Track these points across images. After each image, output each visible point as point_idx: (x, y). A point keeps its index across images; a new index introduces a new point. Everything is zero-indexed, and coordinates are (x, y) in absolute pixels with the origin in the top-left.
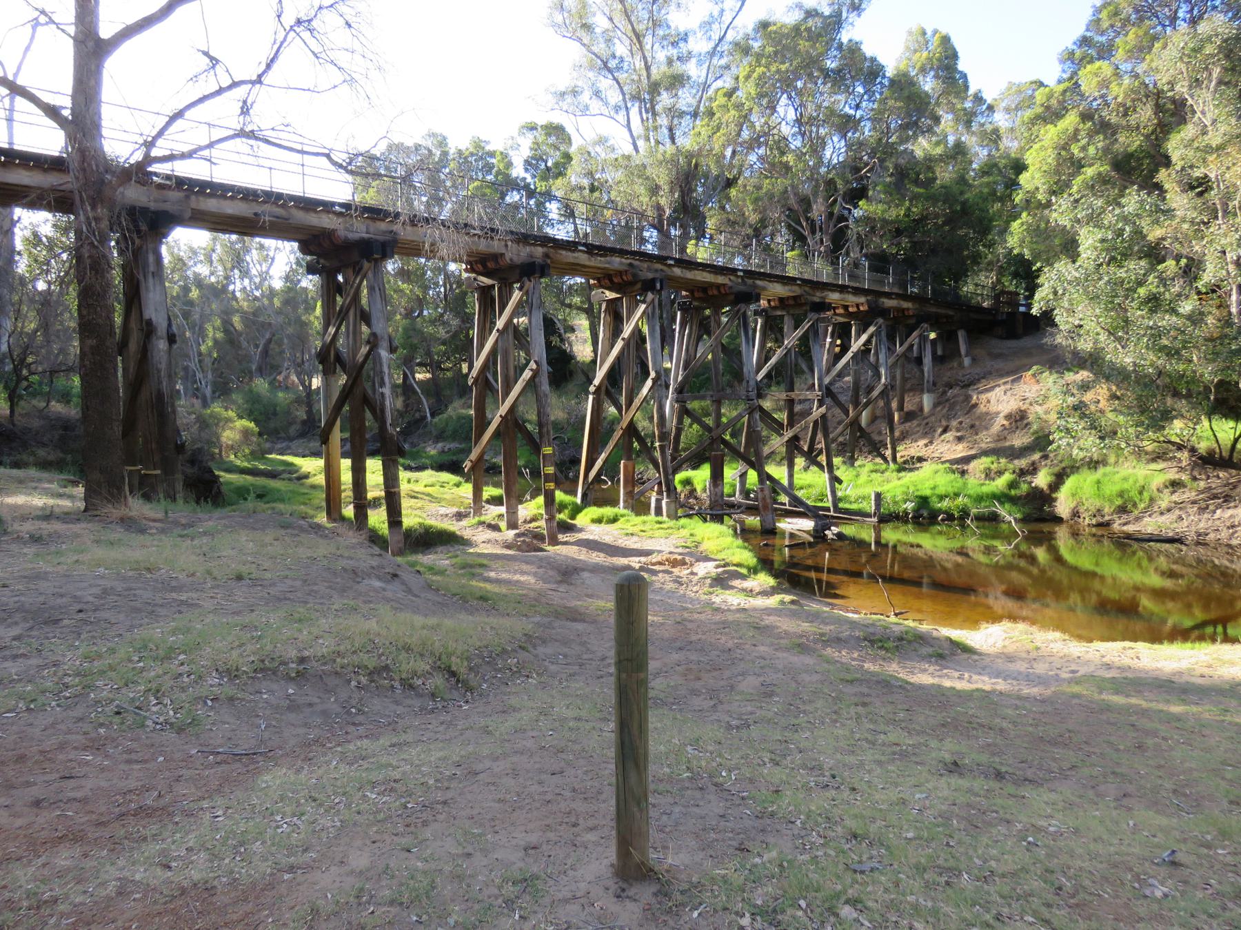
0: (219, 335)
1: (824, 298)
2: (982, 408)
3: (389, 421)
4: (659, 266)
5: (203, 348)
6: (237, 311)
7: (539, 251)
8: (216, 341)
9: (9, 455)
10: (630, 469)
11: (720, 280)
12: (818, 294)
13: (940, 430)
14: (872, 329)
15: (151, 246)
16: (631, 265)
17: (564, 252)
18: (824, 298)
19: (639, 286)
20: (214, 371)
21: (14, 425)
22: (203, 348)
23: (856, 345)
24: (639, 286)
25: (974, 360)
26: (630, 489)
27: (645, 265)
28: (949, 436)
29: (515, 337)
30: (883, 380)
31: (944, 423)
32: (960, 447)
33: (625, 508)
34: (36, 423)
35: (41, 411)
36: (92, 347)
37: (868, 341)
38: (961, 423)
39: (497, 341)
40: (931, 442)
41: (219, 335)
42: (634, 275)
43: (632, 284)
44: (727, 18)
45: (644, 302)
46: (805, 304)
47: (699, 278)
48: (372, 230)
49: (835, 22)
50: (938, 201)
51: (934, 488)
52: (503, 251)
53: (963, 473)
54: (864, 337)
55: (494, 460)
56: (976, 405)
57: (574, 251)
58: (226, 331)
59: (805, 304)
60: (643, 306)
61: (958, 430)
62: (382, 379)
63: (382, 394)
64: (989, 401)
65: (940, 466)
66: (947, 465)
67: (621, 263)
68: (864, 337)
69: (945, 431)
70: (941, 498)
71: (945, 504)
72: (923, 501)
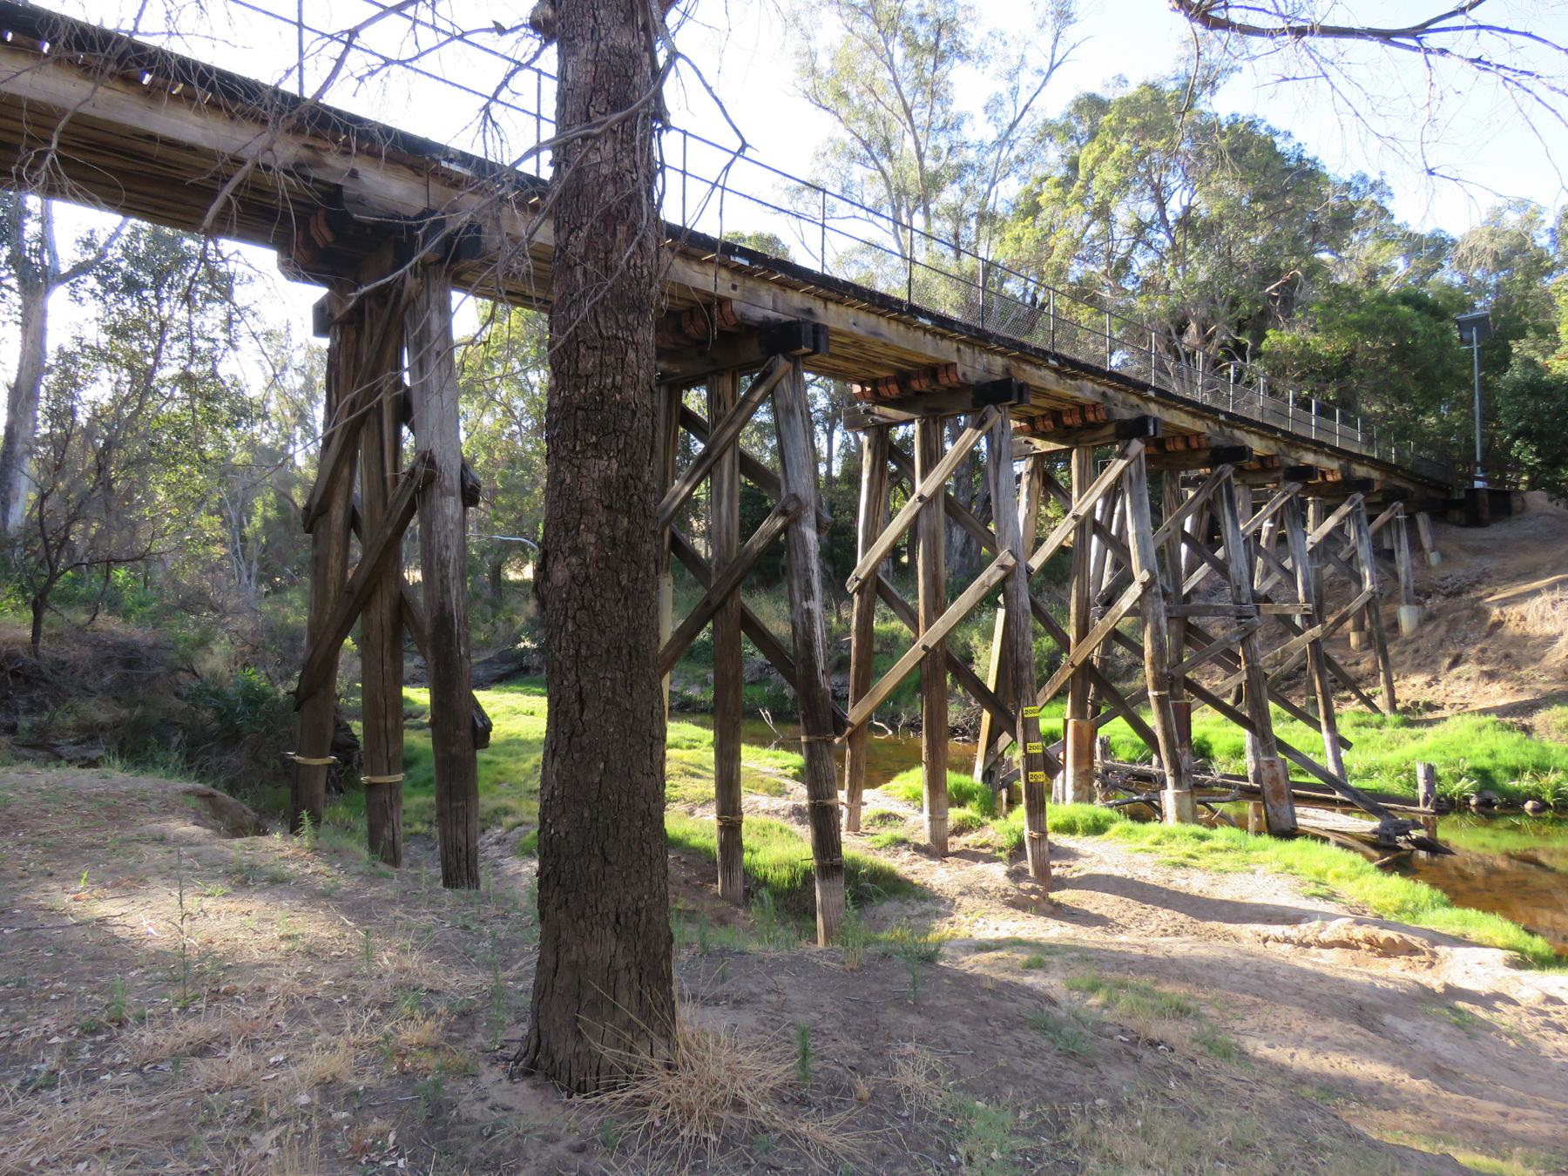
0: (271, 514)
1: (1297, 460)
2: (1512, 629)
3: (821, 666)
4: (1134, 400)
5: (247, 530)
6: (299, 481)
7: (998, 363)
8: (266, 520)
9: (29, 712)
10: (1086, 733)
11: (1198, 426)
12: (1293, 454)
13: (1447, 661)
14: (1345, 509)
15: (434, 296)
16: (1104, 394)
17: (1028, 368)
18: (1297, 460)
19: (1110, 430)
20: (260, 560)
21: (37, 656)
22: (247, 530)
23: (1315, 534)
24: (1110, 430)
25: (1443, 556)
26: (1086, 767)
27: (1120, 396)
28: (1469, 668)
29: (947, 510)
30: (1368, 585)
31: (1454, 651)
32: (1496, 687)
33: (1077, 800)
34: (75, 653)
35: (80, 629)
36: (606, 484)
37: (1339, 528)
38: (1483, 651)
39: (917, 516)
40: (1436, 680)
41: (271, 514)
42: (1109, 412)
43: (1095, 426)
44: (1023, 99)
45: (1122, 455)
46: (1278, 468)
47: (1176, 422)
48: (780, 305)
49: (1188, 94)
50: (1377, 332)
51: (1492, 755)
52: (955, 360)
53: (1527, 730)
54: (1331, 522)
55: (689, 693)
56: (1499, 624)
57: (1039, 367)
58: (280, 509)
59: (1278, 468)
60: (1121, 464)
61: (1481, 662)
62: (809, 583)
63: (809, 612)
64: (1523, 618)
65: (1484, 720)
66: (1493, 717)
67: (1093, 391)
68: (1331, 522)
69: (1456, 662)
70: (1516, 772)
71: (1525, 783)
72: (1484, 776)
